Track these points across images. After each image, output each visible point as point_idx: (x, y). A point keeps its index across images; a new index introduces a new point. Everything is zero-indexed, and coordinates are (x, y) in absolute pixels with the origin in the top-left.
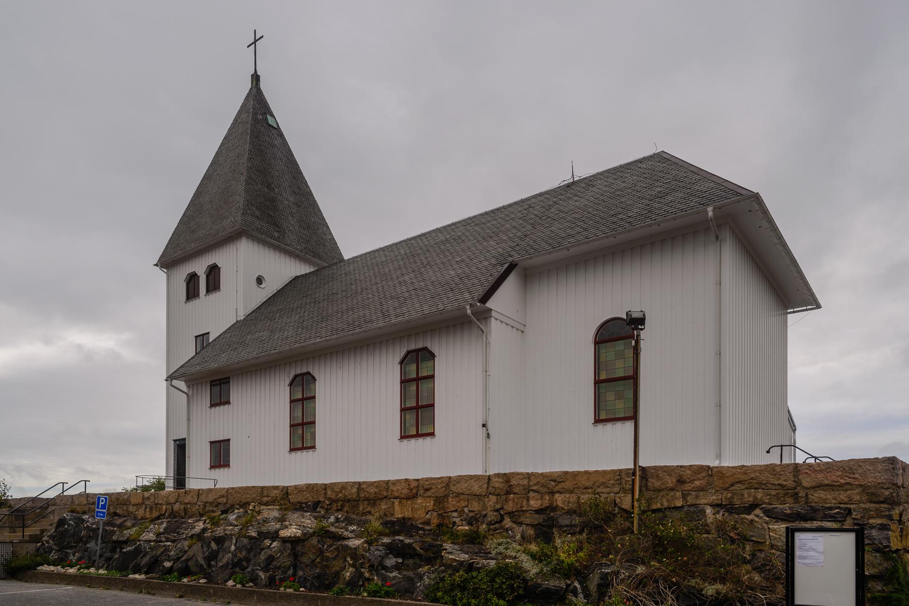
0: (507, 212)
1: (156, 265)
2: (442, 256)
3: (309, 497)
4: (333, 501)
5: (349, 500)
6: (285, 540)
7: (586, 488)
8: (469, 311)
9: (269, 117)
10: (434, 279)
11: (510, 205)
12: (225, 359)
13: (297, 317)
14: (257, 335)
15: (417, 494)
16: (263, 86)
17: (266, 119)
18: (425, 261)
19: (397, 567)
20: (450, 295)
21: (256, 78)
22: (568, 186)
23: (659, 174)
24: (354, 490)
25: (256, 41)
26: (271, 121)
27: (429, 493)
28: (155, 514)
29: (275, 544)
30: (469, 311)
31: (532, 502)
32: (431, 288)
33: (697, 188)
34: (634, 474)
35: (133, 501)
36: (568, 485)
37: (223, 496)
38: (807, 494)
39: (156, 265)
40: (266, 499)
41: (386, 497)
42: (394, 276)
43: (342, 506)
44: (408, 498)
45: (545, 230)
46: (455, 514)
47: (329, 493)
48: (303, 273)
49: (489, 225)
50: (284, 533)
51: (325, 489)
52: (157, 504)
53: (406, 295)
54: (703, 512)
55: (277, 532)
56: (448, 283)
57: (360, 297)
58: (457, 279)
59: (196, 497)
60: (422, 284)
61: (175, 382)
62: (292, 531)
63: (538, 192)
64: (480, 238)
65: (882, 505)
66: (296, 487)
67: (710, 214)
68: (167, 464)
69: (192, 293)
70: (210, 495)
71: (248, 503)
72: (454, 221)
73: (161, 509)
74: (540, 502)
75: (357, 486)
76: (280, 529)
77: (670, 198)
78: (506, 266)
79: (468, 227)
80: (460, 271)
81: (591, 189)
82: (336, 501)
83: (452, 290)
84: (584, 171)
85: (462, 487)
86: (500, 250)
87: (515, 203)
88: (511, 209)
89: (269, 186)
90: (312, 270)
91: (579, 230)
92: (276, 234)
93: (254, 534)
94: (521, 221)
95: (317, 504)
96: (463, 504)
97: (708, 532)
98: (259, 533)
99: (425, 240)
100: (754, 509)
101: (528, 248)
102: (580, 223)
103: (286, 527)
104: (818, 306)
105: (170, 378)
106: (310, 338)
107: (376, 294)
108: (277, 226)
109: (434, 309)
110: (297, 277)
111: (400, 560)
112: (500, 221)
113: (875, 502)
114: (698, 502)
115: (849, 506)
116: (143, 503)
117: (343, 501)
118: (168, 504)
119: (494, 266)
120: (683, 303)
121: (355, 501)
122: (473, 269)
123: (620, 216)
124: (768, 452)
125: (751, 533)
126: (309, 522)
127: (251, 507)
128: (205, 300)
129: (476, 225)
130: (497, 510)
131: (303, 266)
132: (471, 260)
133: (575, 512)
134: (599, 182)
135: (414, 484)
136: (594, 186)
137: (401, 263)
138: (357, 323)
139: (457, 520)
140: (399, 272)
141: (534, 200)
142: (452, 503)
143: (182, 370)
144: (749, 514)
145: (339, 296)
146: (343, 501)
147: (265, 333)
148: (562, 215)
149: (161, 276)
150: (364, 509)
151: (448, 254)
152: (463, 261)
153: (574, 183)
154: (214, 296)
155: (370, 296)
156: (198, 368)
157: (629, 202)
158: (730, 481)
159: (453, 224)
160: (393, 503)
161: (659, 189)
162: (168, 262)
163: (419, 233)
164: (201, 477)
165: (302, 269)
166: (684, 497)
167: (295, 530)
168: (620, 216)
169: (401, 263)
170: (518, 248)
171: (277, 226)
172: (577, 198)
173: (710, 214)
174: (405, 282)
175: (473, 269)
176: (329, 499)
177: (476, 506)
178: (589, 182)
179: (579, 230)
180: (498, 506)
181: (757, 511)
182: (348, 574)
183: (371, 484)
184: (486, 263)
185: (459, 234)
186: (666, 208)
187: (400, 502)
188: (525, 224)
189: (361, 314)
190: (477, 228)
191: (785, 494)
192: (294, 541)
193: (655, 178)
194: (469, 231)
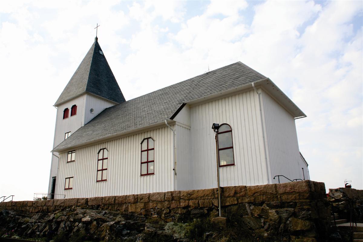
0: (185, 83)
1: (54, 106)
2: (160, 100)
3: (94, 203)
4: (105, 205)
5: (111, 204)
6: (84, 223)
7: (201, 197)
8: (166, 123)
9: (100, 51)
10: (155, 109)
11: (186, 81)
12: (74, 143)
13: (104, 125)
14: (88, 133)
15: (137, 201)
16: (99, 41)
17: (99, 52)
18: (153, 102)
19: (128, 234)
20: (160, 116)
21: (97, 39)
22: (207, 73)
23: (238, 70)
24: (113, 200)
25: (97, 27)
26: (101, 52)
27: (142, 201)
28: (36, 211)
29: (80, 224)
30: (166, 123)
31: (181, 204)
32: (154, 113)
33: (249, 75)
34: (218, 190)
35: (29, 205)
36: (194, 196)
37: (63, 203)
38: (281, 197)
39: (54, 106)
40: (79, 204)
41: (125, 203)
42: (141, 108)
43: (108, 207)
44: (134, 203)
45: (197, 90)
46: (152, 210)
47: (103, 201)
48: (109, 107)
49: (178, 88)
50: (84, 220)
51: (102, 199)
52: (37, 206)
53: (144, 116)
54: (245, 205)
55: (81, 219)
56: (160, 111)
57: (127, 117)
58: (163, 110)
59: (52, 203)
60: (151, 111)
61: (55, 153)
62: (87, 218)
63: (197, 76)
64: (174, 93)
65: (307, 200)
66: (91, 199)
67: (253, 85)
68: (49, 187)
69: (65, 116)
70: (58, 202)
71: (72, 206)
72: (166, 87)
73: (39, 209)
74: (184, 204)
75: (114, 198)
76: (83, 217)
77: (240, 79)
78: (182, 104)
79: (171, 89)
80: (165, 106)
81: (215, 75)
82: (106, 205)
83: (161, 114)
84: (212, 69)
85: (154, 198)
86: (181, 98)
87: (188, 80)
88: (187, 82)
89: (98, 75)
90: (114, 105)
91: (209, 90)
92: (99, 93)
93: (72, 220)
94: (189, 87)
95: (99, 206)
96: (155, 205)
97: (248, 215)
98: (74, 219)
99: (155, 94)
100: (263, 204)
101: (190, 97)
102: (209, 88)
103: (85, 217)
104: (306, 116)
105: (53, 151)
106: (106, 134)
107: (134, 116)
108: (99, 90)
109: (153, 122)
110: (106, 109)
111: (129, 231)
112: (182, 86)
113: (304, 199)
114: (243, 201)
115: (295, 201)
116: (32, 206)
117: (108, 205)
118: (42, 206)
119: (178, 104)
120: (246, 117)
121: (113, 204)
122: (170, 105)
123: (223, 85)
124: (274, 178)
125: (263, 214)
126: (93, 213)
127: (73, 208)
128: (70, 118)
129: (174, 88)
130: (168, 208)
131: (109, 104)
132: (170, 102)
133: (252, 203)
134: (218, 72)
135: (136, 197)
136: (216, 74)
137: (145, 103)
138: (124, 128)
139: (153, 213)
140: (143, 107)
141: (195, 79)
142: (151, 205)
143: (57, 148)
144: (262, 206)
145: (120, 116)
146: (108, 205)
147: (91, 131)
148: (204, 84)
149: (55, 109)
150: (117, 208)
151: (162, 99)
152: (167, 102)
153: (209, 72)
154: (74, 117)
155: (131, 116)
156: (63, 147)
157: (227, 80)
158: (253, 192)
159: (166, 88)
160: (128, 205)
161: (237, 75)
162: (58, 105)
163: (153, 91)
164: (60, 195)
165: (108, 105)
166: (237, 200)
167: (88, 218)
168: (223, 85)
169: (145, 103)
170: (187, 97)
171: (99, 90)
172: (209, 78)
173: (253, 85)
174: (145, 111)
175: (170, 105)
176: (103, 204)
177: (159, 206)
178: (214, 72)
179: (209, 90)
180: (168, 206)
181: (264, 205)
182: (107, 238)
183: (120, 197)
184: (175, 103)
185: (167, 91)
186: (239, 82)
187: (131, 205)
188: (191, 88)
189: (127, 124)
190: (173, 89)
191: (274, 197)
192: (87, 223)
193: (236, 71)
194: (170, 90)
